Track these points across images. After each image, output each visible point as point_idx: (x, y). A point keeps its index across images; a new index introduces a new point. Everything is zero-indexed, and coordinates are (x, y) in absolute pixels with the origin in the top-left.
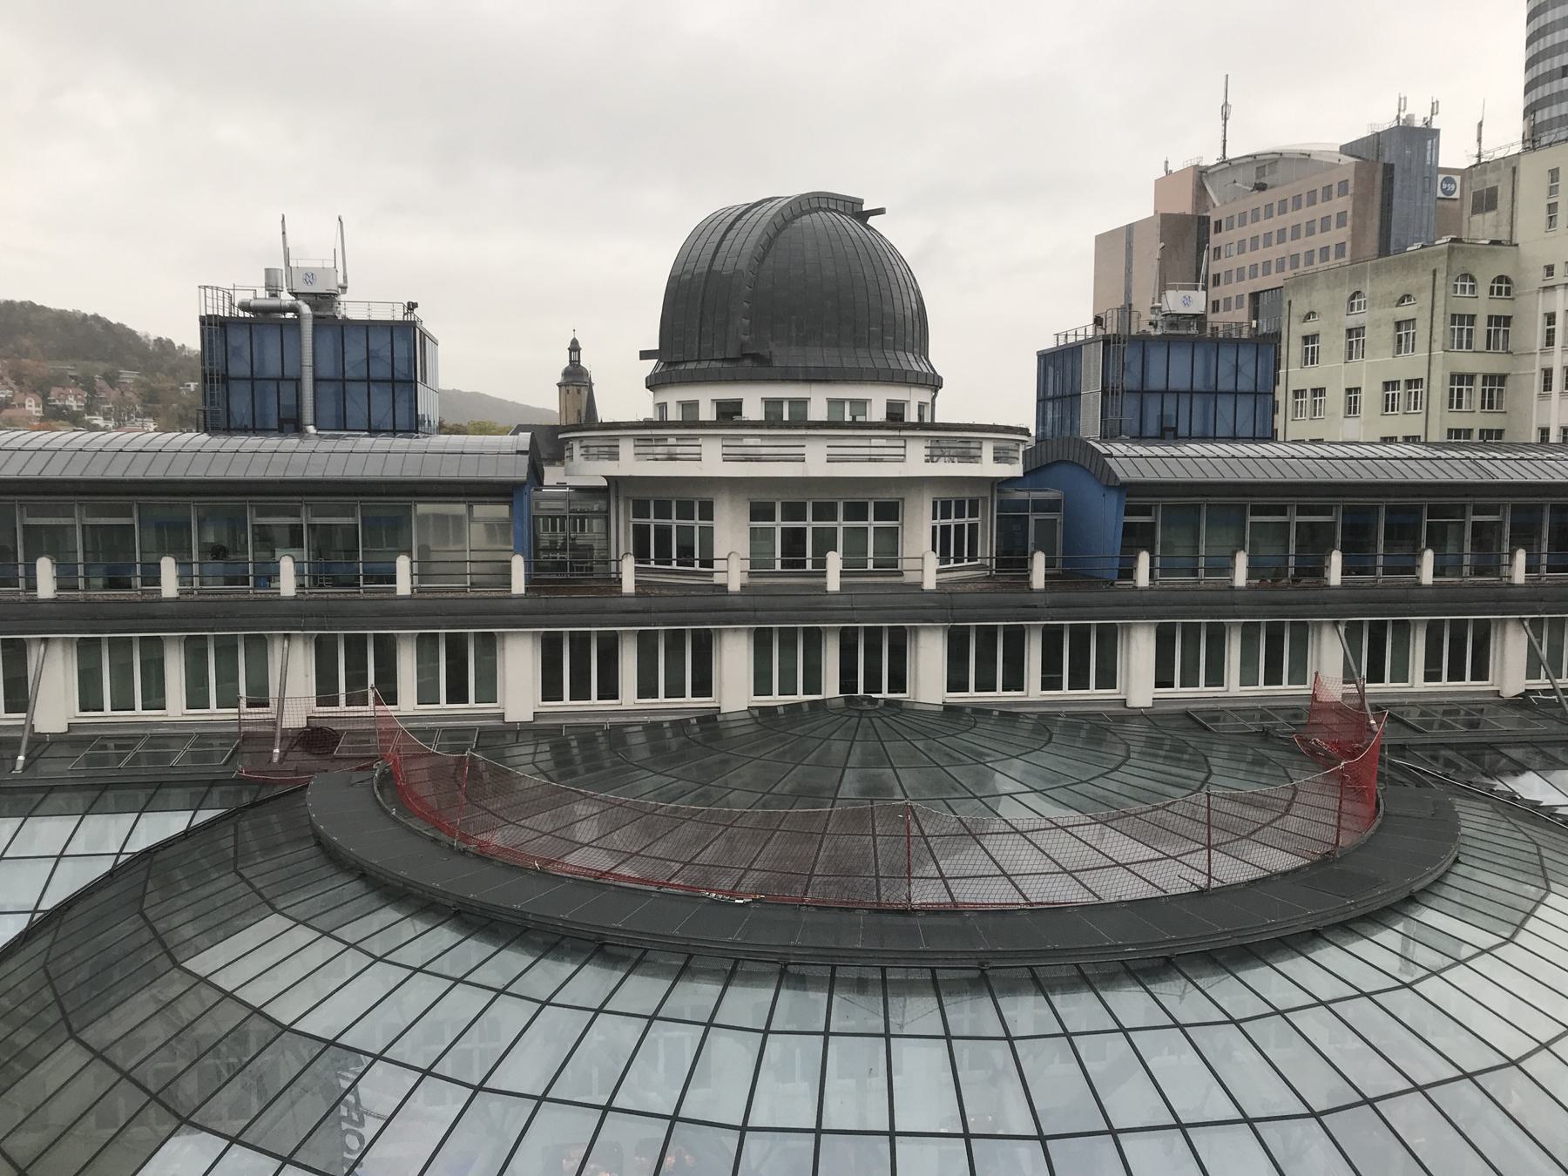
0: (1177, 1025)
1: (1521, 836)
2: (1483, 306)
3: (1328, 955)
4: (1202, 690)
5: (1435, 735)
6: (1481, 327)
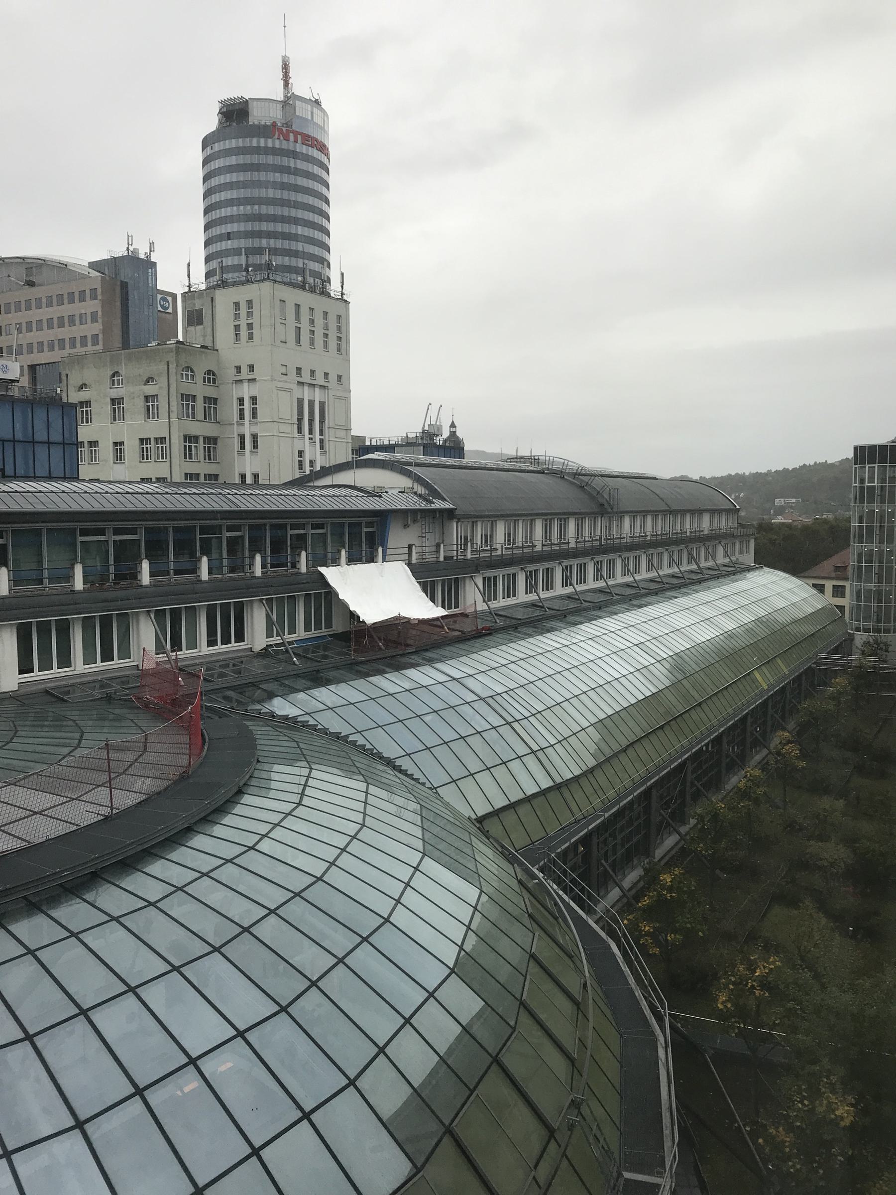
0: (113, 919)
1: (286, 738)
2: (200, 390)
3: (199, 841)
4: (56, 672)
5: (220, 683)
6: (200, 404)
